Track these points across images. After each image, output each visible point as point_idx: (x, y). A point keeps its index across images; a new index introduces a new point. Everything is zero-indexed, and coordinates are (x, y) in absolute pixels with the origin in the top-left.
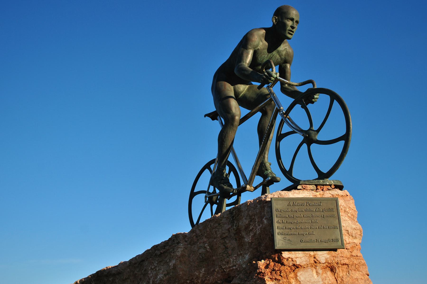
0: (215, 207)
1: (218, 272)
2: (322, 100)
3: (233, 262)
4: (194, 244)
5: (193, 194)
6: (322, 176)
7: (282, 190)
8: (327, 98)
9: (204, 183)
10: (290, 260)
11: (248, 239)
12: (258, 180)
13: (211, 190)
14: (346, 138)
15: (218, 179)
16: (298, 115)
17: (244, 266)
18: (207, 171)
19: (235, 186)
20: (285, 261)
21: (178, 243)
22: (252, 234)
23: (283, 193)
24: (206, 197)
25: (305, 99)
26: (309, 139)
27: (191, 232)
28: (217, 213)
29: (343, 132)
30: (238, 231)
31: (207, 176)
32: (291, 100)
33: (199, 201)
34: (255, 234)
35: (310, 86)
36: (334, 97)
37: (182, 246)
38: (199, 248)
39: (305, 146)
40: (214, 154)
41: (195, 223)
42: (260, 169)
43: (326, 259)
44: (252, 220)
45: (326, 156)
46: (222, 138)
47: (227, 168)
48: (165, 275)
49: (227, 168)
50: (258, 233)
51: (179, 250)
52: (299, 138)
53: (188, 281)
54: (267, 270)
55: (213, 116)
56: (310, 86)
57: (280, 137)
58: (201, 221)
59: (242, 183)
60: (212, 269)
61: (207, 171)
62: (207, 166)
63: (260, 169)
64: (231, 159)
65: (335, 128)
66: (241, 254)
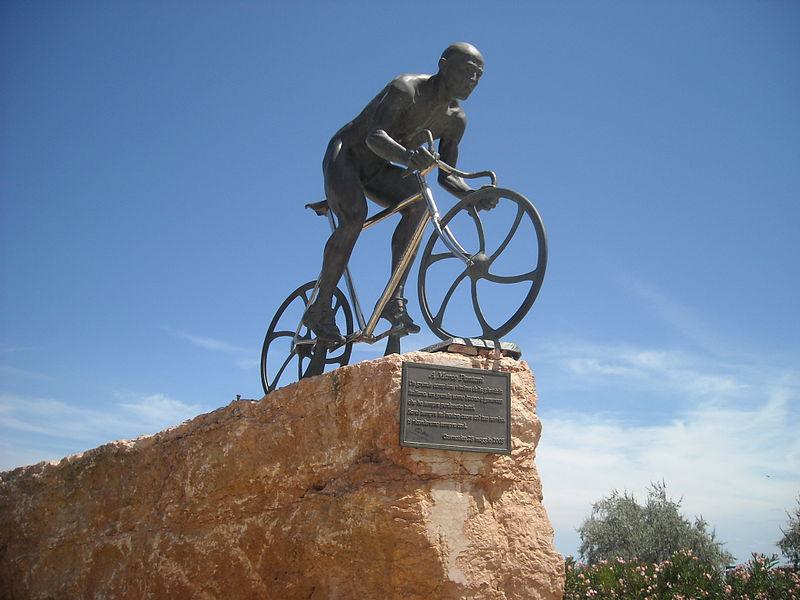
0: (307, 361)
1: (302, 472)
2: (506, 209)
3: (329, 458)
4: (267, 421)
5: (271, 335)
6: (489, 333)
7: (422, 351)
8: (514, 206)
9: (293, 319)
10: (422, 465)
11: (357, 424)
12: (385, 325)
13: (303, 332)
14: (537, 277)
15: (319, 317)
16: (461, 232)
17: (346, 467)
18: (299, 298)
19: (343, 332)
20: (414, 468)
21: (240, 417)
22: (364, 416)
23: (423, 355)
24: (293, 343)
25: (479, 201)
26: (478, 270)
27: (265, 400)
28: (309, 373)
29: (533, 267)
30: (343, 409)
31: (298, 308)
32: (455, 200)
33: (281, 348)
34: (369, 418)
35: (485, 182)
36: (524, 207)
37: (247, 424)
38: (276, 429)
39: (467, 279)
40: (314, 272)
41: (344, 346)
42: (392, 309)
43: (479, 469)
44: (367, 395)
45: (500, 302)
46: (342, 268)
47: (334, 299)
48: (214, 466)
49: (334, 299)
50: (375, 415)
51: (242, 428)
52: (459, 266)
53: (251, 481)
54: (356, 211)
55: (320, 208)
56: (485, 182)
57: (428, 259)
58: (281, 384)
59: (356, 328)
60: (293, 466)
61: (299, 298)
62: (301, 292)
63: (392, 309)
64: (342, 285)
65: (520, 258)
66: (343, 448)
